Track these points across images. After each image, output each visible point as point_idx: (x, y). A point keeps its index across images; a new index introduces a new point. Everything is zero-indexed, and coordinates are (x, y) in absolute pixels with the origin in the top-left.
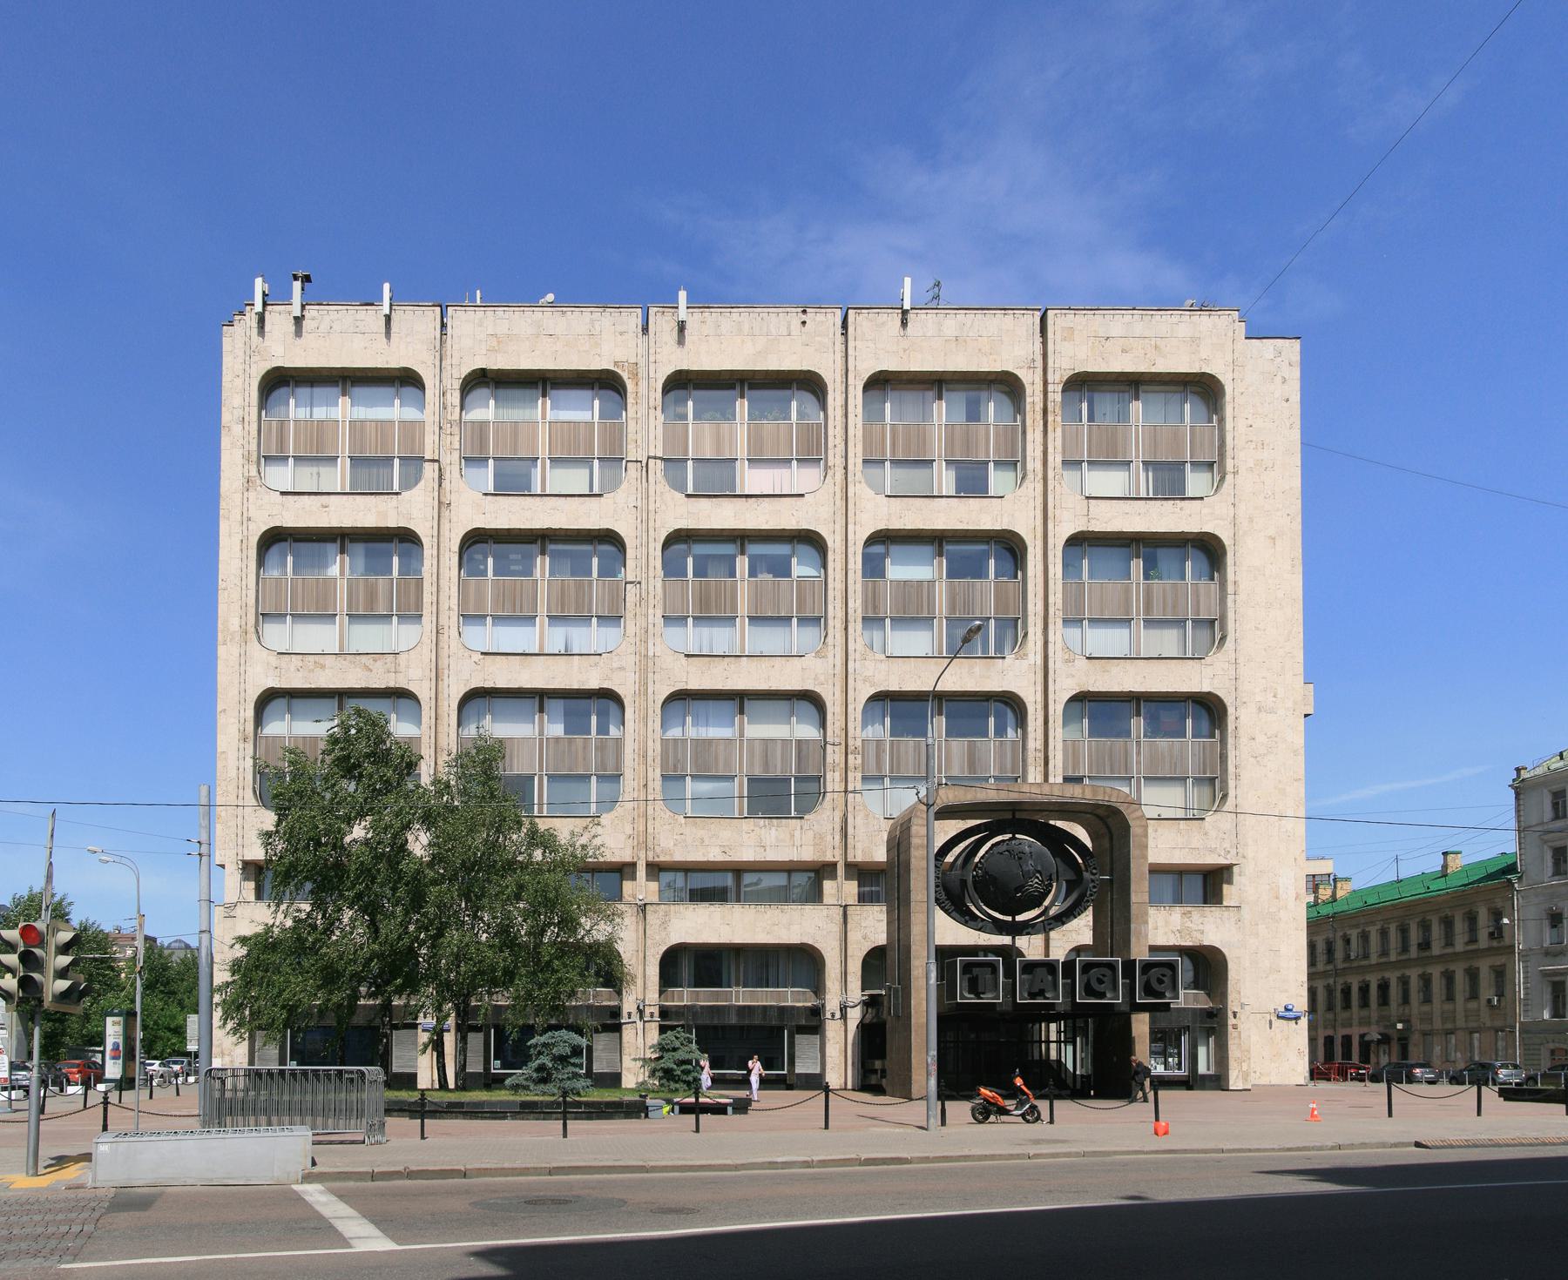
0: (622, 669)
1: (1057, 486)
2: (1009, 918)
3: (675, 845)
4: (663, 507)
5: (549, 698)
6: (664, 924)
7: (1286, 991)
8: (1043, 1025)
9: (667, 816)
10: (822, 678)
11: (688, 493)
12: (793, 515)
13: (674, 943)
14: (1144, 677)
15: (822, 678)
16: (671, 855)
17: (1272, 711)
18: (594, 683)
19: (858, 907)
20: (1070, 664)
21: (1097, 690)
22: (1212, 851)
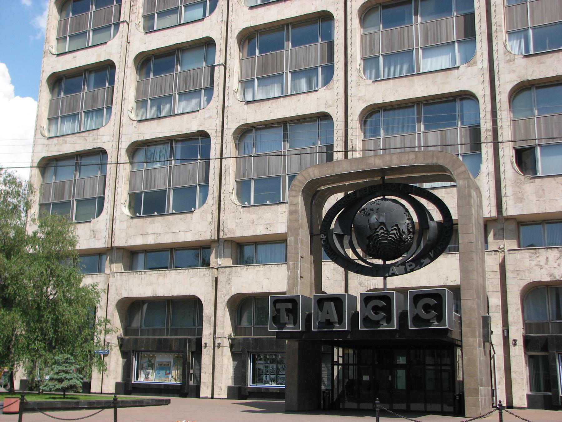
0: (210, 117)
3: (236, 226)
4: (237, 17)
6: (229, 280)
9: (232, 207)
10: (330, 103)
12: (312, 4)
15: (330, 103)
16: (234, 233)
20: (511, 63)
21: (535, 78)
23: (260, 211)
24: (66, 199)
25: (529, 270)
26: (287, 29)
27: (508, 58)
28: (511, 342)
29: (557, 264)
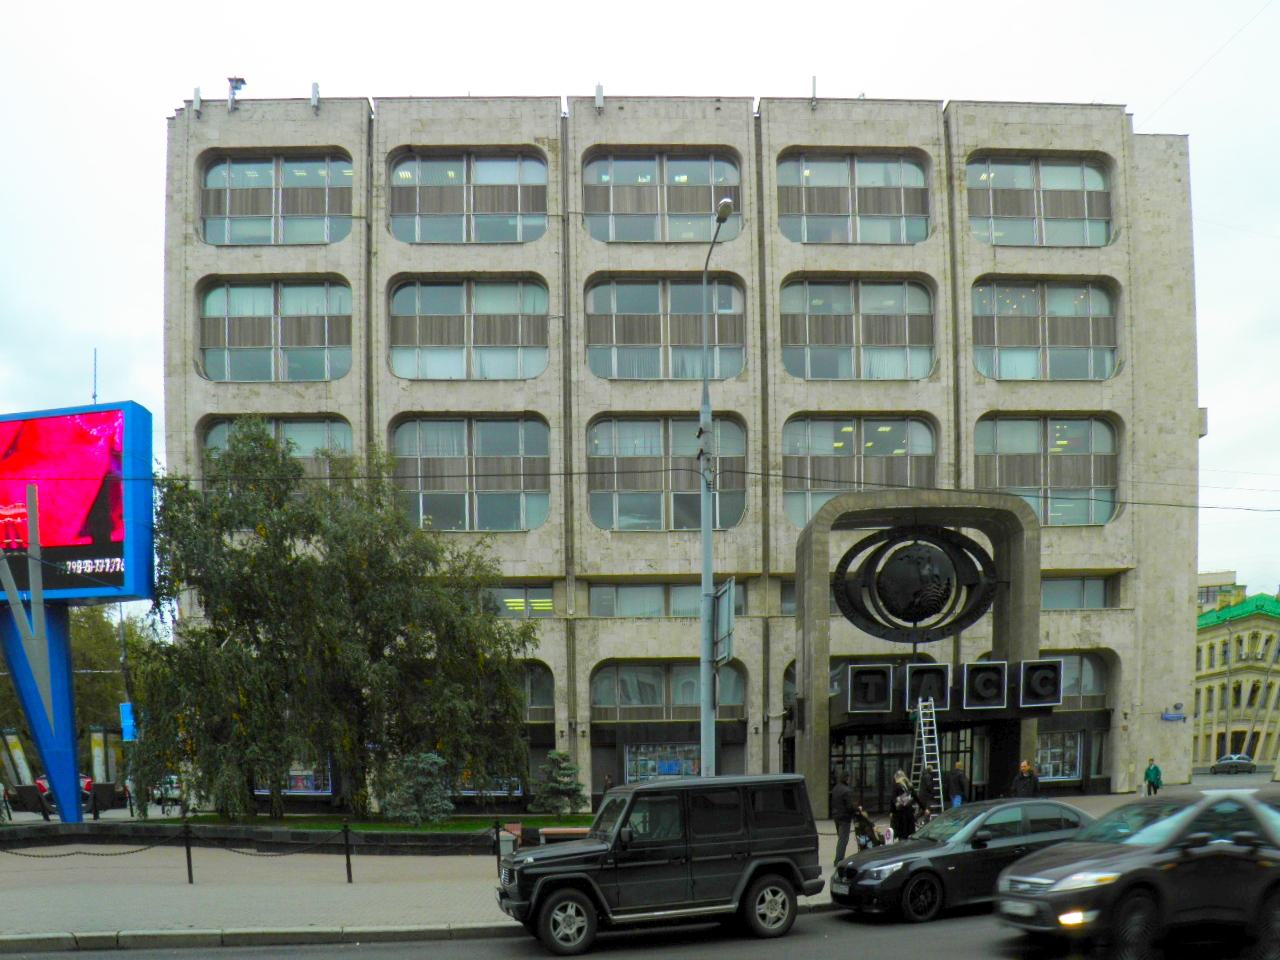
0: (546, 393)
1: (965, 237)
2: (910, 625)
5: (478, 421)
6: (593, 639)
11: (611, 240)
13: (604, 658)
15: (743, 400)
16: (598, 569)
17: (1171, 431)
18: (519, 406)
19: (781, 619)
22: (1111, 557)
23: (639, 540)
26: (664, 285)
27: (977, 380)
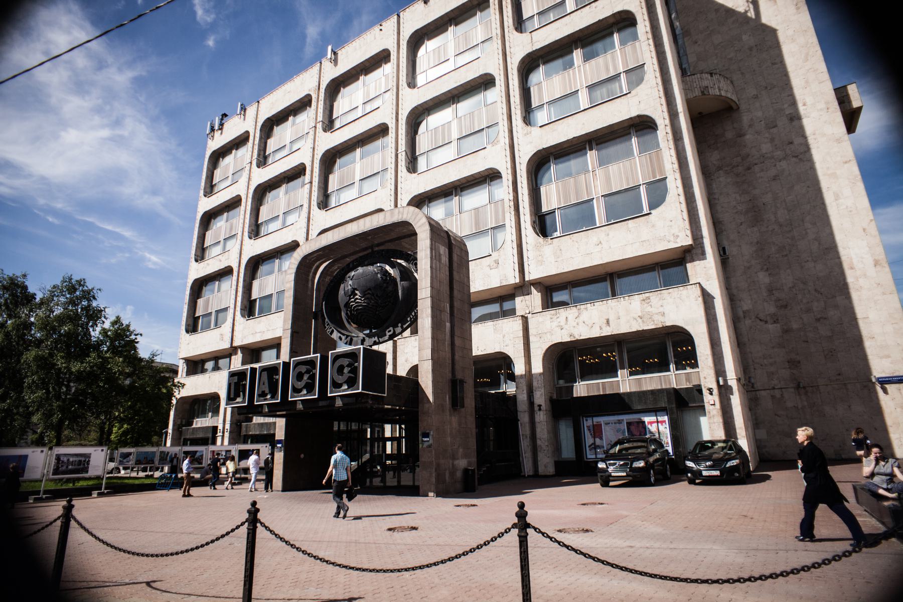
7: (888, 356)
8: (349, 423)
14: (583, 124)
24: (210, 311)
25: (551, 332)
27: (525, 132)
28: (536, 408)
29: (576, 323)
